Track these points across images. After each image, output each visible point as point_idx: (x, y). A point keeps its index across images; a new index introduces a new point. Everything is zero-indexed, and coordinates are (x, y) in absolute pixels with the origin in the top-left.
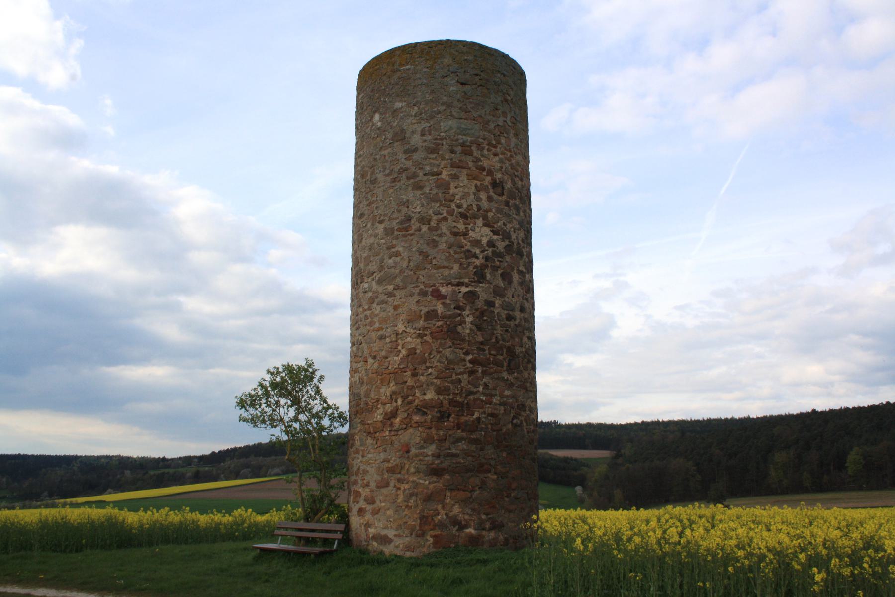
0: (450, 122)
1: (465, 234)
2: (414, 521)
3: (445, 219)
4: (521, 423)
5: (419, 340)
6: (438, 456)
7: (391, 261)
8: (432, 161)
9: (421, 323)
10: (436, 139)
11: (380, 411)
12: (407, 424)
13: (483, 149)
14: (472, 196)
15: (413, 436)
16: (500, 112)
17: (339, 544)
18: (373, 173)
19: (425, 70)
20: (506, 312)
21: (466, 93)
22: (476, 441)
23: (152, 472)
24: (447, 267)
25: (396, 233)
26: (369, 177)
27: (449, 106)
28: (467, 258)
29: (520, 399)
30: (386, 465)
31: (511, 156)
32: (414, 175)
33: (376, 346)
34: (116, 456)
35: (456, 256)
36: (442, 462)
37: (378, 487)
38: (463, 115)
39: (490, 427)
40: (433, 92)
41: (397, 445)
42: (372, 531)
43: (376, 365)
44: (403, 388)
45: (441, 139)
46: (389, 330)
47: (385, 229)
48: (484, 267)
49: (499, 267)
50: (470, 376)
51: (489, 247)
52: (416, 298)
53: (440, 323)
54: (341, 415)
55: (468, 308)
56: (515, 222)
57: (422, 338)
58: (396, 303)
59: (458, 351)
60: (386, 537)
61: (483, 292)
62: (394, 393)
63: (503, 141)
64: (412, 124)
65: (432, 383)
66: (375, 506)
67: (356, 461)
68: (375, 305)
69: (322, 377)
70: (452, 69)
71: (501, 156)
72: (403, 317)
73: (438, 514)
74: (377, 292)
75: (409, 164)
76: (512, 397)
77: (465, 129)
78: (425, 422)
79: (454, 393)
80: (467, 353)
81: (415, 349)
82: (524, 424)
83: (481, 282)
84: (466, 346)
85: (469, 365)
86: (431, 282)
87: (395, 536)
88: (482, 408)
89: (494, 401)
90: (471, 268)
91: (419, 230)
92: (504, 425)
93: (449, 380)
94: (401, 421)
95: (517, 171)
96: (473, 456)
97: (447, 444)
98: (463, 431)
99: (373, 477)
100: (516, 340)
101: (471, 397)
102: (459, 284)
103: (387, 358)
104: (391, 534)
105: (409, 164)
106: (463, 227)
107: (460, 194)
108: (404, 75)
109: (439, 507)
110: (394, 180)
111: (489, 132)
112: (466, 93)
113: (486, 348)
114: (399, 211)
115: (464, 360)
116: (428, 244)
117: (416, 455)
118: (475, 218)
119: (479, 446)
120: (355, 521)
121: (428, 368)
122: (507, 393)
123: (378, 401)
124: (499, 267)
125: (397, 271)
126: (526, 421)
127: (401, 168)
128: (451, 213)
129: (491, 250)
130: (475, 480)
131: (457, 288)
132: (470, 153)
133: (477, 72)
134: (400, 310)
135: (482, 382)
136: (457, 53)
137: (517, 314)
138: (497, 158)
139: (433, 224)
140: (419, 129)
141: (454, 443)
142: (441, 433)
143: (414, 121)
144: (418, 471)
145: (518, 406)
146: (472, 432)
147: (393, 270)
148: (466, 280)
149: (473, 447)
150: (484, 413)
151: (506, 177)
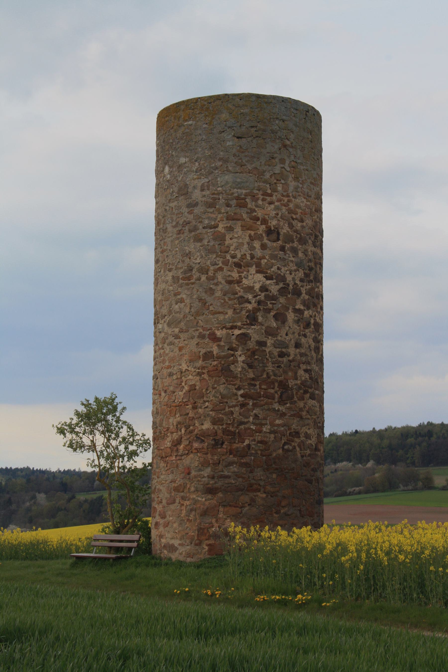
0: (227, 177)
1: (239, 282)
2: (193, 533)
3: (221, 269)
4: (294, 448)
5: (198, 378)
6: (213, 478)
7: (177, 307)
8: (210, 215)
9: (200, 363)
10: (213, 194)
11: (169, 439)
13: (258, 199)
14: (246, 246)
15: (193, 460)
16: (277, 160)
17: (135, 552)
18: (164, 223)
19: (205, 126)
21: (241, 147)
22: (246, 465)
23: (81, 497)
25: (181, 281)
26: (161, 226)
27: (225, 161)
28: (240, 304)
30: (173, 485)
31: (289, 201)
34: (22, 470)
35: (230, 302)
36: (216, 483)
37: (168, 504)
38: (237, 169)
39: (259, 452)
40: (211, 148)
41: (181, 468)
42: (163, 541)
43: (167, 398)
45: (218, 194)
46: (175, 368)
47: (173, 277)
48: (256, 310)
50: (241, 408)
52: (196, 341)
53: (215, 363)
55: (240, 348)
56: (291, 264)
57: (201, 376)
58: (181, 345)
59: (230, 386)
60: (173, 545)
62: (179, 423)
63: (280, 188)
64: (194, 179)
65: (208, 415)
66: (166, 520)
67: (154, 482)
68: (166, 345)
69: (124, 408)
71: (277, 204)
72: (186, 357)
74: (166, 333)
78: (203, 448)
79: (227, 424)
80: (239, 389)
81: (195, 385)
82: (298, 449)
84: (238, 382)
85: (240, 399)
86: (208, 326)
87: (180, 544)
89: (264, 429)
90: (244, 312)
91: (199, 279)
93: (222, 412)
94: (184, 448)
96: (243, 478)
98: (235, 456)
99: (164, 495)
100: (290, 374)
101: (242, 427)
102: (232, 328)
103: (174, 392)
104: (176, 543)
105: (191, 217)
106: (237, 275)
107: (235, 245)
108: (187, 130)
109: (214, 521)
110: (179, 232)
111: (265, 182)
112: (241, 147)
113: (258, 383)
114: (183, 261)
115: (236, 395)
116: (206, 292)
117: (195, 477)
118: (248, 266)
119: (249, 469)
120: (154, 533)
121: (205, 402)
122: (278, 422)
123: (168, 430)
125: (182, 316)
126: (299, 446)
127: (185, 221)
128: (226, 263)
129: (263, 294)
130: (245, 498)
132: (245, 205)
133: (253, 124)
135: (252, 414)
137: (292, 351)
138: (272, 206)
139: (211, 274)
140: (199, 185)
141: (226, 466)
143: (195, 177)
144: (197, 490)
145: (290, 434)
146: (243, 457)
147: (178, 315)
148: (239, 324)
150: (254, 440)
151: (281, 223)
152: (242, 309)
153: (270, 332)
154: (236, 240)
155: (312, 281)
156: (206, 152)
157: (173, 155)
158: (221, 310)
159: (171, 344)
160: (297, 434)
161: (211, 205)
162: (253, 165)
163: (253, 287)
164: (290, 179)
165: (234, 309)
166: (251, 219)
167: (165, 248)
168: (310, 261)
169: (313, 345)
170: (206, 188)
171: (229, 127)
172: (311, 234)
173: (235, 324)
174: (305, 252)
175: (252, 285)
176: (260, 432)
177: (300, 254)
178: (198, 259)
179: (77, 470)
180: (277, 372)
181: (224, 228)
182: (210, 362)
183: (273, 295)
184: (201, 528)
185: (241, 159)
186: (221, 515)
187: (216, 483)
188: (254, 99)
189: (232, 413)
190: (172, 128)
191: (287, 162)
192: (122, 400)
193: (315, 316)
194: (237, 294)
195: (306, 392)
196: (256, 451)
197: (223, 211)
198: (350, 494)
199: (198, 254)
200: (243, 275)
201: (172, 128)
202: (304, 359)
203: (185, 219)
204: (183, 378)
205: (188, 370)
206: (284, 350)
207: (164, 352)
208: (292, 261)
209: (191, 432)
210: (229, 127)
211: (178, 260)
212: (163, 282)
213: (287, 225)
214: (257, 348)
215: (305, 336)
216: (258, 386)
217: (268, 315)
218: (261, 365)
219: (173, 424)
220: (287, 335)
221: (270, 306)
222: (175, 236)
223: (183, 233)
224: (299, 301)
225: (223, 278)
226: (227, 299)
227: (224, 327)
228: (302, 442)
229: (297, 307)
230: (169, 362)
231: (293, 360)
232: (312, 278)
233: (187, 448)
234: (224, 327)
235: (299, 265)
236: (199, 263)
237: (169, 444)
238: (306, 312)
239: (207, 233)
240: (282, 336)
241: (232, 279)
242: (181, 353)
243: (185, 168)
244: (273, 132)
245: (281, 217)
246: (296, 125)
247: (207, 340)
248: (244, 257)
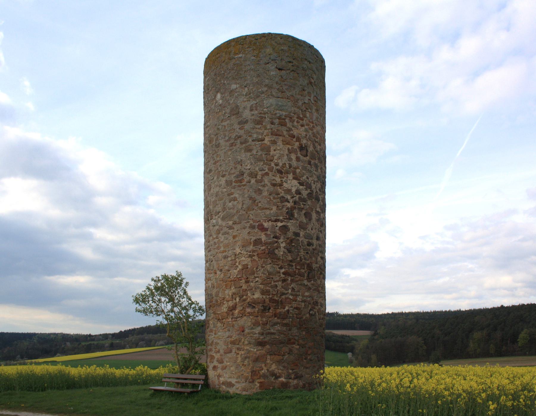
0: (271, 100)
1: (281, 185)
2: (247, 373)
3: (267, 174)
4: (315, 313)
5: (250, 259)
6: (263, 334)
7: (230, 204)
8: (258, 130)
9: (251, 247)
10: (261, 113)
11: (226, 306)
12: (243, 314)
13: (294, 121)
14: (286, 157)
15: (246, 322)
16: (306, 92)
17: (202, 387)
18: (217, 139)
19: (253, 58)
20: (307, 240)
21: (282, 77)
22: (286, 325)
23: (83, 344)
24: (268, 209)
25: (234, 184)
26: (214, 143)
28: (282, 202)
31: (313, 127)
32: (246, 141)
34: (60, 334)
35: (274, 201)
36: (264, 338)
37: (225, 353)
38: (280, 95)
39: (295, 316)
40: (258, 76)
41: (236, 327)
42: (222, 379)
43: (222, 275)
45: (265, 114)
46: (230, 252)
48: (293, 208)
50: (283, 283)
53: (263, 248)
54: (200, 308)
55: (282, 237)
57: (252, 257)
58: (234, 234)
59: (275, 266)
61: (292, 226)
62: (234, 293)
63: (308, 115)
67: (211, 337)
68: (220, 235)
70: (272, 57)
71: (306, 127)
72: (239, 243)
73: (262, 369)
75: (242, 132)
76: (310, 297)
77: (281, 106)
78: (254, 312)
79: (272, 294)
80: (281, 268)
81: (247, 265)
82: (317, 314)
83: (291, 219)
84: (280, 263)
85: (282, 276)
86: (258, 219)
87: (236, 382)
89: (298, 299)
90: (284, 209)
91: (249, 182)
92: (304, 315)
93: (269, 285)
94: (239, 312)
96: (284, 334)
98: (278, 318)
99: (222, 347)
100: (314, 259)
101: (283, 297)
102: (276, 221)
103: (229, 271)
104: (233, 381)
105: (242, 132)
106: (280, 180)
107: (277, 155)
108: (238, 62)
109: (263, 365)
110: (232, 145)
111: (298, 108)
112: (282, 77)
113: (294, 264)
114: (236, 168)
115: (279, 272)
116: (255, 192)
117: (249, 333)
118: (287, 173)
119: (288, 328)
120: (211, 373)
121: (255, 277)
122: (307, 294)
123: (224, 299)
125: (235, 211)
126: (318, 312)
128: (271, 169)
129: (298, 196)
130: (286, 349)
131: (275, 223)
132: (285, 125)
134: (237, 239)
136: (276, 45)
137: (314, 242)
138: (303, 128)
139: (259, 177)
140: (249, 106)
141: (272, 326)
142: (264, 319)
143: (245, 99)
144: (250, 343)
146: (284, 319)
147: (232, 210)
148: (281, 218)
150: (292, 307)
151: (309, 143)
152: (283, 206)
154: (278, 152)
156: (254, 79)
157: (225, 84)
158: (267, 206)
159: (225, 233)
162: (290, 93)
165: (278, 207)
166: (289, 136)
167: (218, 159)
170: (254, 108)
171: (272, 60)
173: (278, 218)
175: (290, 188)
178: (248, 166)
180: (306, 256)
181: (269, 141)
182: (259, 247)
184: (254, 371)
185: (282, 86)
186: (268, 361)
187: (264, 338)
188: (290, 40)
189: (276, 286)
190: (224, 62)
194: (279, 194)
196: (293, 314)
197: (268, 127)
199: (249, 162)
201: (224, 62)
203: (237, 134)
204: (237, 259)
205: (241, 253)
206: (310, 241)
207: (219, 240)
210: (272, 60)
211: (231, 167)
212: (217, 186)
214: (294, 237)
216: (294, 267)
217: (301, 213)
218: (296, 251)
219: (229, 295)
221: (302, 206)
222: (228, 148)
223: (236, 145)
225: (269, 181)
226: (272, 198)
227: (270, 220)
230: (224, 248)
233: (242, 312)
234: (270, 220)
236: (249, 169)
237: (225, 310)
241: (275, 182)
242: (234, 240)
243: (236, 92)
244: (303, 69)
247: (257, 229)
248: (284, 166)
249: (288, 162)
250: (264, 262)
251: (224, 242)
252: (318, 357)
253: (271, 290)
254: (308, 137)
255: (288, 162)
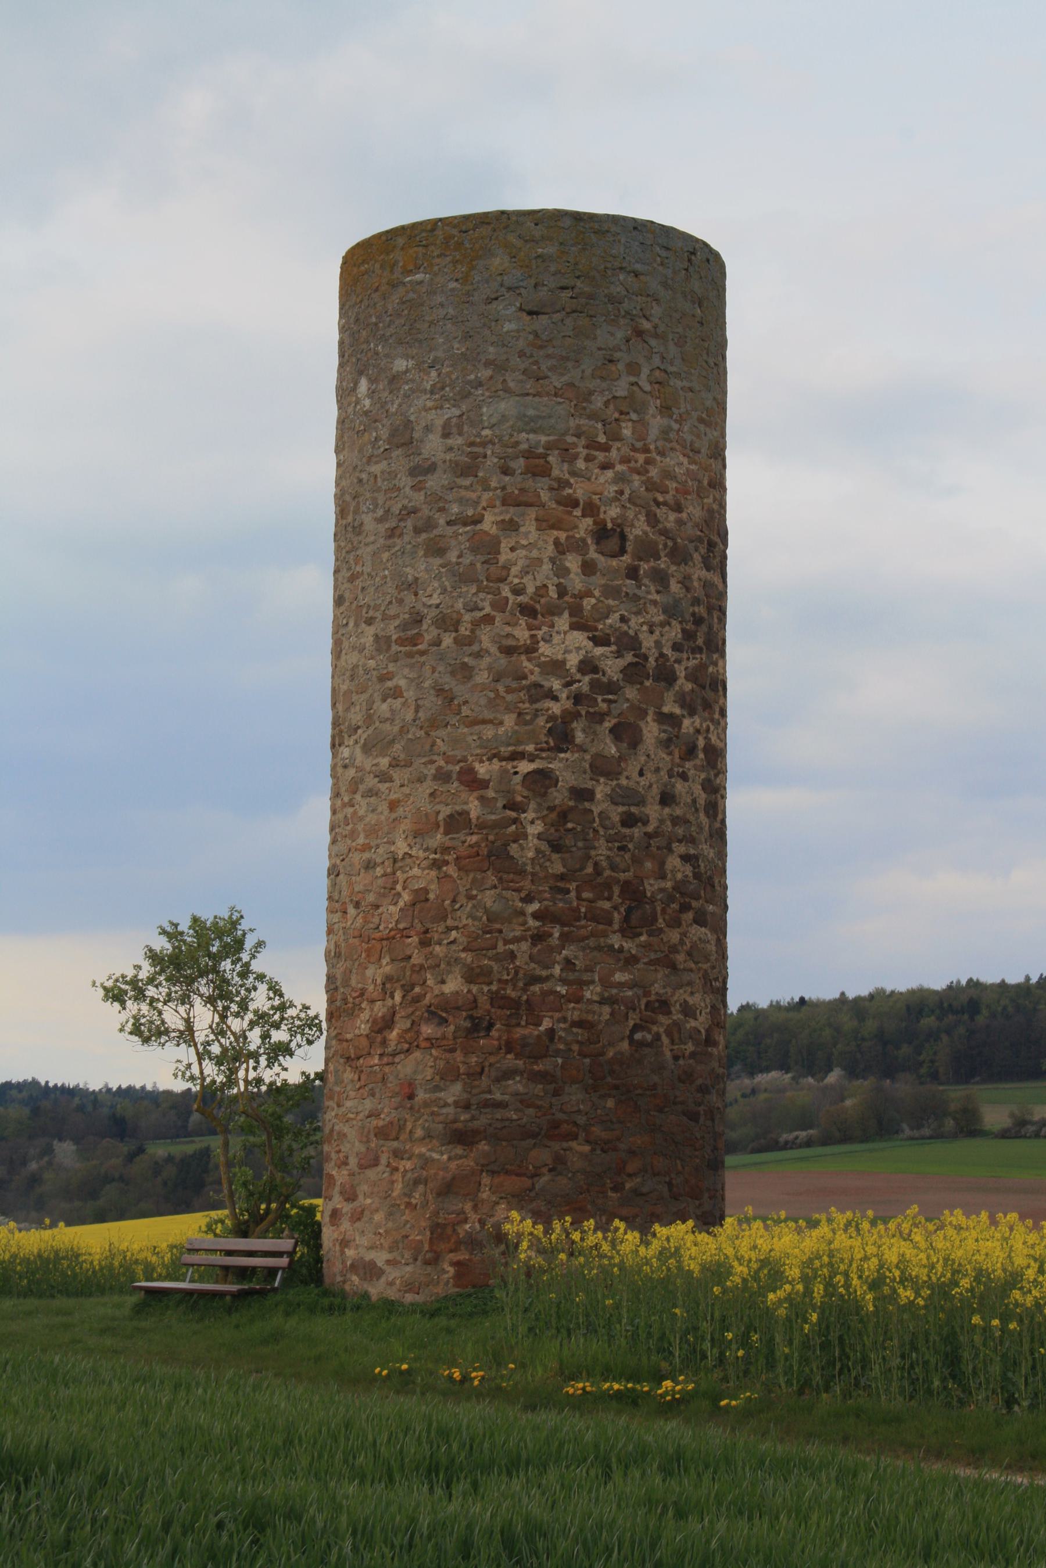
0: (503, 405)
1: (530, 650)
2: (420, 1236)
3: (488, 620)
4: (657, 1037)
5: (433, 873)
6: (467, 1107)
7: (384, 707)
8: (463, 493)
9: (439, 838)
10: (472, 444)
11: (365, 1015)
12: (411, 1044)
13: (576, 457)
14: (547, 567)
15: (417, 1066)
16: (621, 366)
17: (283, 1279)
18: (356, 512)
19: (453, 285)
20: (621, 809)
21: (537, 335)
22: (543, 1077)
23: (159, 1150)
24: (490, 722)
26: (350, 518)
27: (500, 367)
28: (533, 700)
29: (657, 988)
31: (648, 462)
33: (361, 881)
34: (21, 1086)
35: (509, 698)
36: (473, 1118)
37: (362, 1167)
38: (529, 386)
39: (575, 1047)
40: (467, 336)
41: (392, 1084)
42: (350, 1253)
44: (404, 968)
45: (484, 444)
46: (381, 851)
47: (377, 637)
48: (569, 717)
49: (608, 713)
50: (534, 945)
51: (584, 674)
52: (429, 786)
53: (474, 838)
54: (312, 1023)
55: (533, 805)
56: (652, 610)
57: (439, 868)
58: (393, 796)
59: (508, 894)
60: (372, 1264)
62: (388, 979)
63: (627, 432)
65: (457, 960)
66: (356, 1204)
67: (330, 1117)
68: (358, 797)
69: (260, 944)
70: (508, 280)
71: (619, 468)
72: (406, 825)
73: (466, 1220)
76: (632, 985)
77: (532, 419)
78: (444, 1038)
79: (500, 981)
80: (528, 899)
81: (426, 891)
82: (665, 1040)
83: (562, 751)
84: (526, 884)
85: (532, 923)
86: (458, 754)
87: (388, 1262)
88: (560, 1010)
89: (588, 995)
90: (541, 721)
91: (437, 643)
92: (611, 1044)
93: (490, 953)
94: (400, 1036)
95: (665, 492)
96: (538, 1107)
97: (485, 1081)
98: (518, 1056)
99: (353, 1147)
100: (649, 865)
101: (536, 988)
102: (515, 756)
103: (377, 907)
104: (380, 1258)
105: (419, 498)
108: (411, 295)
109: (468, 1207)
110: (392, 533)
111: (593, 416)
112: (537, 335)
114: (400, 601)
115: (522, 913)
116: (453, 673)
117: (426, 1104)
118: (553, 614)
121: (449, 929)
122: (619, 977)
123: (362, 995)
124: (608, 713)
125: (396, 729)
126: (669, 1033)
127: (404, 507)
128: (500, 605)
129: (587, 679)
130: (542, 1155)
131: (509, 766)
132: (544, 471)
133: (564, 282)
134: (400, 811)
136: (519, 243)
137: (653, 811)
138: (610, 474)
139: (464, 630)
140: (439, 422)
141: (498, 1080)
142: (473, 1059)
143: (429, 404)
144: (429, 1136)
145: (647, 1005)
146: (536, 1058)
147: (387, 726)
148: (530, 748)
149: (538, 1089)
150: (564, 1019)
151: (630, 514)
152: (536, 713)
153: (602, 768)
155: (700, 650)
156: (456, 346)
157: (377, 353)
158: (488, 715)
159: (371, 793)
160: (664, 1006)
161: (466, 470)
163: (564, 662)
164: (652, 410)
165: (520, 714)
166: (559, 503)
167: (359, 569)
168: (696, 601)
169: (702, 797)
170: (454, 430)
171: (509, 289)
172: (700, 540)
173: (520, 749)
174: (685, 582)
175: (560, 657)
176: (578, 1000)
177: (674, 587)
178: (435, 596)
179: (149, 1087)
181: (497, 523)
182: (461, 836)
183: (610, 682)
184: (438, 1225)
185: (536, 363)
188: (568, 222)
189: (512, 955)
190: (377, 290)
191: (645, 371)
192: (255, 925)
193: (708, 730)
194: (525, 677)
195: (685, 908)
197: (493, 484)
198: (786, 1146)
200: (540, 634)
201: (377, 290)
202: (680, 831)
204: (399, 873)
205: (411, 856)
206: (634, 809)
207: (355, 813)
208: (655, 603)
209: (417, 999)
210: (509, 289)
211: (388, 598)
213: (643, 518)
215: (684, 777)
216: (573, 894)
218: (580, 844)
220: (641, 774)
221: (604, 706)
222: (382, 541)
223: (401, 535)
224: (669, 696)
225: (494, 642)
226: (501, 689)
227: (495, 756)
228: (675, 1023)
229: (666, 709)
230: (367, 837)
231: (656, 834)
232: (700, 641)
233: (408, 1036)
234: (495, 756)
235: (671, 611)
236: (438, 606)
237: (364, 1028)
238: (686, 722)
239: (456, 535)
240: (630, 777)
241: (514, 643)
242: (393, 816)
244: (612, 299)
245: (630, 500)
246: (665, 285)
247: (456, 784)
248: (542, 592)
249: (556, 580)
250: (474, 881)
251: (368, 819)
252: (670, 1184)
253: (495, 968)
254: (626, 495)
255: (556, 580)
